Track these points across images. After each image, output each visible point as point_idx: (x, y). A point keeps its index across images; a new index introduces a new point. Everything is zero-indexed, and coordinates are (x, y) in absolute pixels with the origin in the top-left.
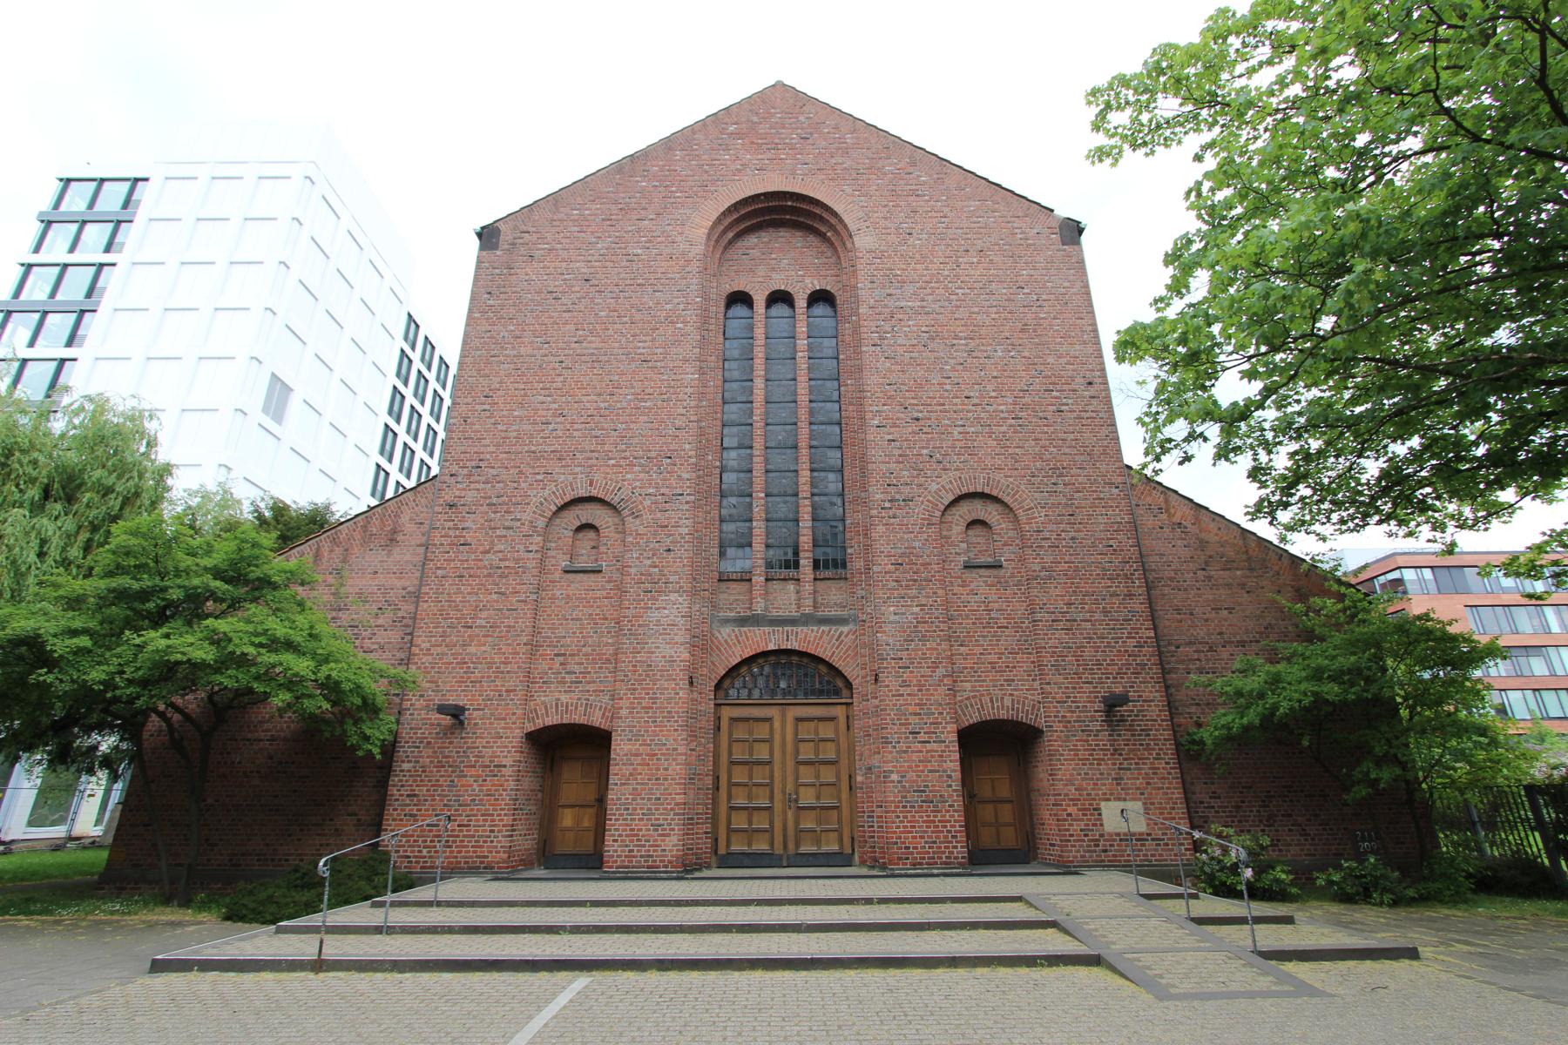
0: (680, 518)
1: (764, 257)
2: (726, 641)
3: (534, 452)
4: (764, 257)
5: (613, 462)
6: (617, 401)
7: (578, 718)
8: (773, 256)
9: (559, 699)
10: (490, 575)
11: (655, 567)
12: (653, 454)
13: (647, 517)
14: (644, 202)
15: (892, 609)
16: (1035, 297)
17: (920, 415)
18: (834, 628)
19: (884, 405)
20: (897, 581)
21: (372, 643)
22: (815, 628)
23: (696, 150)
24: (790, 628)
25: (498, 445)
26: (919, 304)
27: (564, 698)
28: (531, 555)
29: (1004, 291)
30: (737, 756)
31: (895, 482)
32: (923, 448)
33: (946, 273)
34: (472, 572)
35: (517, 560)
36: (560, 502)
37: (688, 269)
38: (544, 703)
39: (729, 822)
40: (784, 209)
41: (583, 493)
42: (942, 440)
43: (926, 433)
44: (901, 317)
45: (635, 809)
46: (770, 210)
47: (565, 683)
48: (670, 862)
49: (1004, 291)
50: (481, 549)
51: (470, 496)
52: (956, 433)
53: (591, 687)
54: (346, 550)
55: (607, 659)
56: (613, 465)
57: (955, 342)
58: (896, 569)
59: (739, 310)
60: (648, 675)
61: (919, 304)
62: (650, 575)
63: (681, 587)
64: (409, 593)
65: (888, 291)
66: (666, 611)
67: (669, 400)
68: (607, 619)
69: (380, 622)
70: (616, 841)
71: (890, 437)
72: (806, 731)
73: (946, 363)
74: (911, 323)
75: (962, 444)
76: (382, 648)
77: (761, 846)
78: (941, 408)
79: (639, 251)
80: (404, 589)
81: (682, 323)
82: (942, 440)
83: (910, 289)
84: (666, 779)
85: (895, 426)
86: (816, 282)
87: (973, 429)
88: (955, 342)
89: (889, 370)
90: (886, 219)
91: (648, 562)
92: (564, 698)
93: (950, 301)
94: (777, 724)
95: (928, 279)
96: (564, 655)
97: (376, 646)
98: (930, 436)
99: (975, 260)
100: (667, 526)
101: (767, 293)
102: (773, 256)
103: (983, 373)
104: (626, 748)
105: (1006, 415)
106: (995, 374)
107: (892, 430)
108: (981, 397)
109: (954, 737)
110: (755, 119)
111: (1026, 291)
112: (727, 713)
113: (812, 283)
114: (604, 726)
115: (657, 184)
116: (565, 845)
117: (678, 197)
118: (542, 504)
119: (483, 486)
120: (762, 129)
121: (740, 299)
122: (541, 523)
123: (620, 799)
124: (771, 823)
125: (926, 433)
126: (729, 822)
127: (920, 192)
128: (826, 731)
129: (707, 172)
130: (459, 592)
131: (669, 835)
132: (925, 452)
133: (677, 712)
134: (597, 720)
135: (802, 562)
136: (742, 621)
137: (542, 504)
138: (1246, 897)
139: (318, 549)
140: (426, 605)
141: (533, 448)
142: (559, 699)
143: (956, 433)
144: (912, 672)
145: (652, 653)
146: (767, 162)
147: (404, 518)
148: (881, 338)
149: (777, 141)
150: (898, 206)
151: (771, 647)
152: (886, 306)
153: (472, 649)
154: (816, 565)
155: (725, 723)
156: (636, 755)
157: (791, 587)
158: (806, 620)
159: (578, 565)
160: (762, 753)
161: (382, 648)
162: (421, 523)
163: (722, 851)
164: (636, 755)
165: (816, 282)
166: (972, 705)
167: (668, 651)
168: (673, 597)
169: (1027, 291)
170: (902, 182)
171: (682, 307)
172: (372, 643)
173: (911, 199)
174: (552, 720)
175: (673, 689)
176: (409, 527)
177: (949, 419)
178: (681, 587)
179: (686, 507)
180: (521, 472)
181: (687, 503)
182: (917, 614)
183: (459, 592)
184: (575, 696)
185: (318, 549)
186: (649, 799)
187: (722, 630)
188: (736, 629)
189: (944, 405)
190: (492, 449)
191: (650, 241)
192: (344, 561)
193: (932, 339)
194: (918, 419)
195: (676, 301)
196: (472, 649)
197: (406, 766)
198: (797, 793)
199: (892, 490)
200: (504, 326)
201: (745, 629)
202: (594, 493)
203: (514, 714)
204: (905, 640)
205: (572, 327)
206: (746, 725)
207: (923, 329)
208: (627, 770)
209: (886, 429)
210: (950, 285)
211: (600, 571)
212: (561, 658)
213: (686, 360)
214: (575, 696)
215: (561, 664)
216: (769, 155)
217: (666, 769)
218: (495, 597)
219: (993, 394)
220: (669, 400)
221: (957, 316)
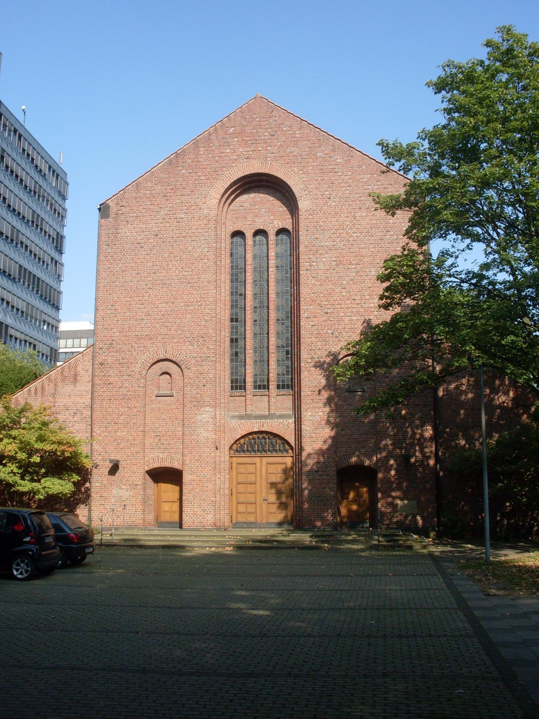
0: (209, 369)
1: (252, 207)
2: (234, 427)
3: (137, 335)
4: (252, 207)
5: (176, 340)
6: (176, 307)
7: (167, 464)
8: (257, 207)
9: (158, 456)
10: (123, 399)
11: (198, 394)
12: (195, 336)
13: (194, 369)
14: (184, 184)
15: (309, 413)
16: (396, 237)
17: (329, 311)
18: (285, 421)
19: (310, 305)
20: (312, 400)
21: (74, 429)
22: (276, 420)
23: (212, 146)
24: (264, 421)
25: (120, 332)
26: (332, 243)
27: (161, 455)
28: (141, 389)
29: (379, 234)
30: (240, 480)
31: (314, 348)
32: (329, 329)
33: (348, 223)
34: (115, 397)
35: (135, 392)
36: (152, 362)
37: (209, 226)
38: (152, 457)
39: (237, 509)
40: (262, 181)
41: (162, 357)
42: (339, 324)
43: (331, 321)
44: (322, 252)
45: (194, 503)
46: (250, 182)
47: (161, 448)
48: (210, 524)
49: (379, 234)
50: (118, 386)
51: (110, 360)
52: (346, 320)
53: (172, 451)
54: (55, 385)
55: (179, 438)
56: (176, 342)
57: (349, 267)
58: (312, 394)
59: (238, 239)
60: (197, 446)
61: (332, 243)
62: (196, 398)
63: (210, 404)
64: (86, 405)
65: (315, 236)
66: (204, 416)
67: (201, 305)
68: (177, 419)
69: (75, 419)
70: (187, 516)
71: (313, 324)
72: (242, 469)
73: (344, 279)
74: (326, 256)
75: (349, 326)
76: (78, 431)
77: (251, 519)
78: (339, 306)
79: (183, 216)
80: (84, 403)
81: (207, 259)
82: (339, 324)
83: (328, 234)
84: (207, 491)
85: (315, 317)
86: (280, 223)
87: (355, 318)
88: (349, 267)
89: (314, 285)
90: (317, 189)
91: (195, 392)
92: (161, 455)
93: (348, 241)
94: (258, 465)
95: (337, 227)
96: (159, 436)
97: (75, 431)
98: (333, 322)
99: (365, 214)
100: (203, 373)
101: (253, 231)
102: (257, 207)
103: (363, 285)
104: (189, 478)
105: (373, 309)
106: (370, 285)
107: (314, 319)
108: (361, 299)
109: (334, 473)
110: (245, 123)
111: (390, 233)
112: (235, 460)
113: (278, 224)
114: (179, 467)
115: (191, 171)
116: (166, 517)
117: (202, 179)
118: (143, 363)
119: (115, 354)
120: (248, 130)
121: (238, 234)
122: (144, 373)
123: (187, 499)
124: (256, 509)
125: (331, 321)
126: (237, 509)
127: (336, 170)
128: (251, 468)
129: (217, 162)
130: (110, 407)
131: (209, 514)
132: (330, 331)
133: (211, 462)
134: (176, 465)
135: (270, 387)
136: (241, 417)
137: (143, 363)
138: (488, 544)
139: (43, 384)
140: (96, 413)
141: (137, 333)
142: (158, 456)
143: (346, 320)
144: (317, 444)
145: (199, 435)
146: (251, 153)
147: (79, 368)
148: (311, 265)
149: (257, 138)
150: (323, 180)
151: (256, 430)
152: (314, 246)
153: (119, 434)
154: (278, 387)
155: (234, 465)
156: (194, 481)
157: (266, 399)
158: (270, 416)
159: (162, 392)
160: (252, 478)
161: (78, 431)
162: (87, 371)
163: (234, 521)
164: (194, 481)
165: (280, 223)
166: (345, 459)
167: (205, 434)
168: (207, 408)
169: (392, 233)
170: (327, 163)
171: (206, 250)
172: (74, 429)
173: (331, 174)
174: (156, 465)
175: (209, 452)
176: (82, 373)
177: (343, 313)
178: (210, 404)
179: (211, 364)
180: (132, 347)
181: (212, 361)
182: (321, 416)
183: (110, 407)
184: (166, 454)
185: (43, 384)
186: (200, 499)
187: (232, 421)
188: (239, 421)
189: (341, 304)
190: (118, 334)
191: (188, 209)
192: (55, 390)
193: (337, 265)
194: (327, 313)
195: (203, 246)
196: (119, 434)
197: (97, 484)
198: (267, 497)
199: (312, 352)
200: (117, 264)
201: (243, 421)
202: (168, 357)
203: (140, 463)
204: (315, 429)
205: (150, 264)
206: (244, 466)
207: (333, 259)
208: (190, 487)
209: (311, 320)
210: (349, 231)
211: (173, 396)
212: (158, 437)
213: (209, 282)
214: (166, 454)
215: (159, 440)
216: (252, 149)
217: (207, 487)
218: (126, 409)
219: (368, 297)
220: (201, 305)
221: (352, 250)
